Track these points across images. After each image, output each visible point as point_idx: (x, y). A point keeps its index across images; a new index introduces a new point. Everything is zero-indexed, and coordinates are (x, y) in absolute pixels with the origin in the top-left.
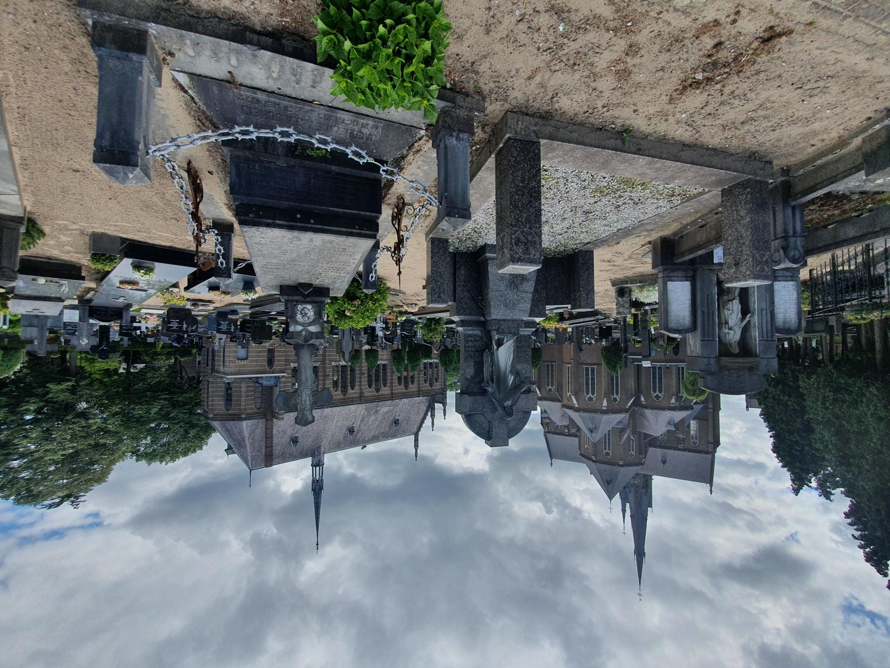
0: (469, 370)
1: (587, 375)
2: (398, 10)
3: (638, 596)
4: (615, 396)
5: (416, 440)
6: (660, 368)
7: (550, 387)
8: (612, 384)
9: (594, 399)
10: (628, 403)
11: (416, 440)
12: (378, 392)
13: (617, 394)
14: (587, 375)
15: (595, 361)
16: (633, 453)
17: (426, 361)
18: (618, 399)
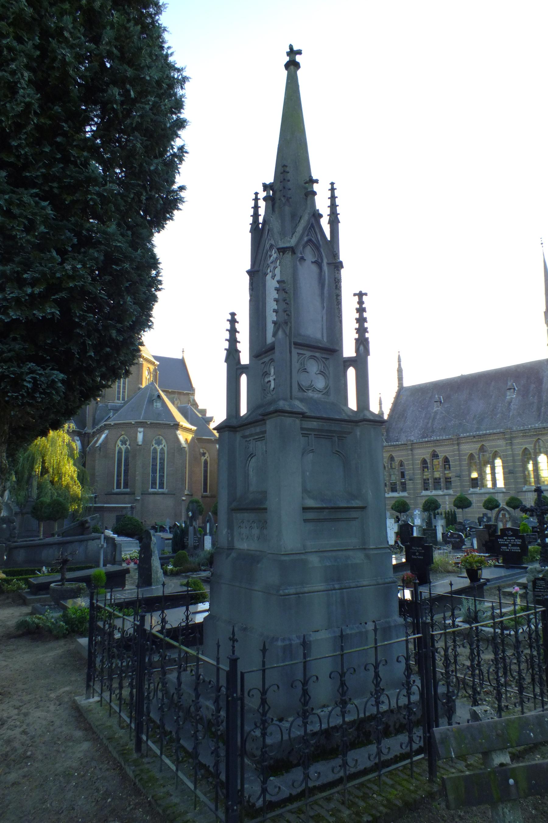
1: (162, 477)
4: (123, 448)
5: (400, 379)
8: (127, 465)
9: (154, 442)
10: (106, 437)
11: (400, 379)
12: (434, 451)
13: (120, 452)
14: (162, 477)
15: (152, 498)
17: (405, 494)
18: (119, 443)
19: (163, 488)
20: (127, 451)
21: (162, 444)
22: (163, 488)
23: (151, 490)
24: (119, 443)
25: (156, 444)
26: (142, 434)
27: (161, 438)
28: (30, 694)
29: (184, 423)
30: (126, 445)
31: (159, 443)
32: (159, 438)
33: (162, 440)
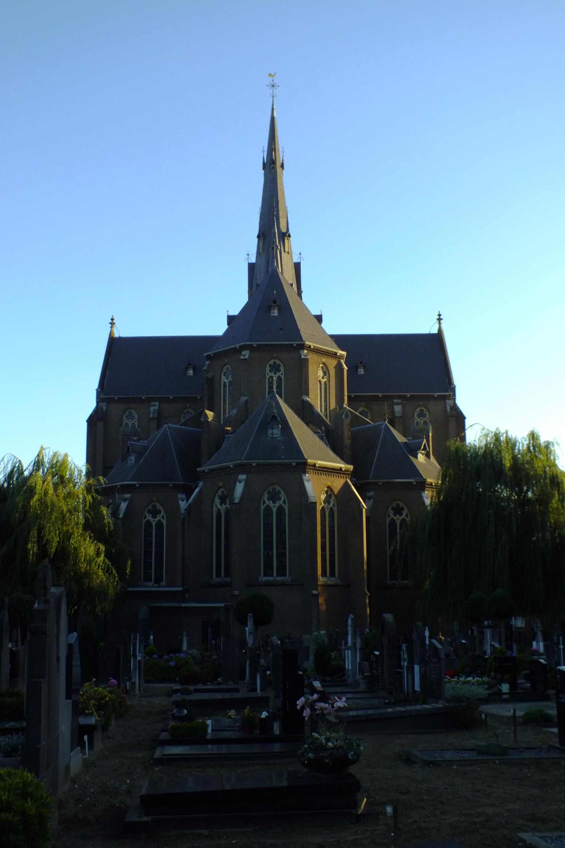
0: (34, 501)
1: (281, 555)
2: (479, 448)
3: (269, 91)
6: (147, 578)
7: (398, 519)
9: (266, 496)
14: (281, 555)
16: (224, 379)
19: (284, 575)
20: (227, 512)
21: (279, 499)
22: (284, 575)
23: (263, 579)
24: (217, 501)
25: (269, 499)
26: (243, 484)
27: (278, 488)
28: (356, 634)
29: (169, 396)
30: (225, 504)
31: (274, 497)
32: (274, 489)
33: (279, 492)
